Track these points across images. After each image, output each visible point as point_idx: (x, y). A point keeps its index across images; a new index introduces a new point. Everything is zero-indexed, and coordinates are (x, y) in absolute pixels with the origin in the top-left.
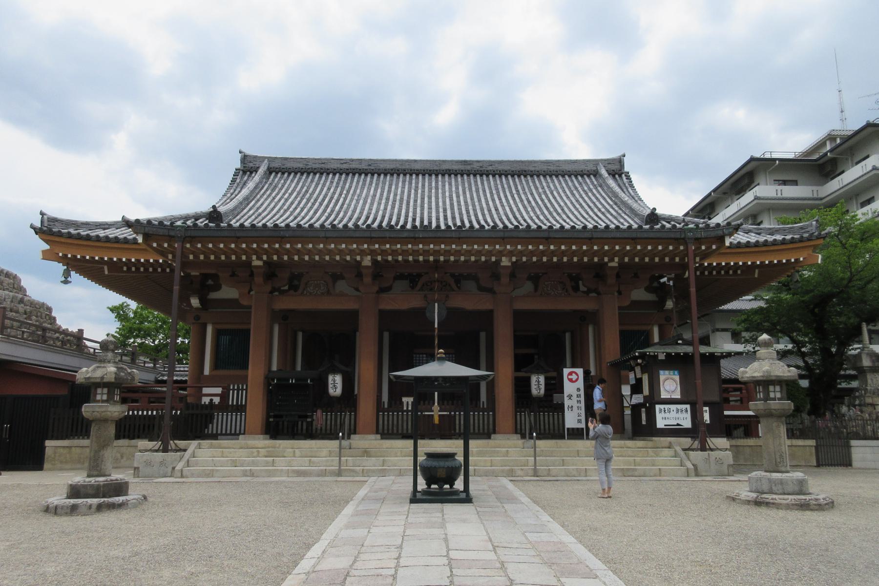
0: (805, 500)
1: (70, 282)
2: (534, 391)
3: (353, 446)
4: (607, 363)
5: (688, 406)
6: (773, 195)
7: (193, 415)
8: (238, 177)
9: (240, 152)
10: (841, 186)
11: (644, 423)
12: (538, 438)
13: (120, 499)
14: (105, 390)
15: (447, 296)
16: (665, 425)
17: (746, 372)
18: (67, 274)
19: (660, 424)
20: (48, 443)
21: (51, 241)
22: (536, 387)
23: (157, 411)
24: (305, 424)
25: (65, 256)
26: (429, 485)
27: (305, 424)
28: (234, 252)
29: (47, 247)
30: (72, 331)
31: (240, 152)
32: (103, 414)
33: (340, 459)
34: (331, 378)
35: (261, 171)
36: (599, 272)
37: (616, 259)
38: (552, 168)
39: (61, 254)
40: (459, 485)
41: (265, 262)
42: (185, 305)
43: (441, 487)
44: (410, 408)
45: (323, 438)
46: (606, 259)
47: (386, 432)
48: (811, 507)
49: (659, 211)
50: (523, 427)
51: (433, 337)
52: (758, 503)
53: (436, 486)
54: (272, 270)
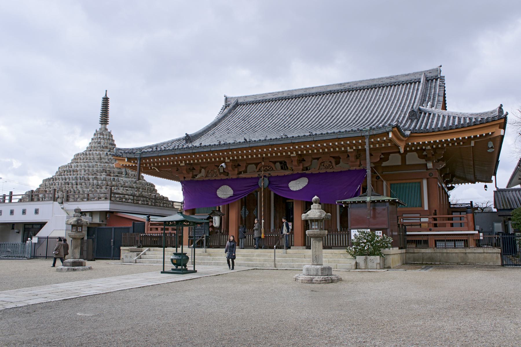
3: (287, 252)
20: (122, 248)
23: (158, 234)
28: (337, 146)
38: (393, 80)
41: (231, 160)
46: (289, 153)
49: (189, 133)
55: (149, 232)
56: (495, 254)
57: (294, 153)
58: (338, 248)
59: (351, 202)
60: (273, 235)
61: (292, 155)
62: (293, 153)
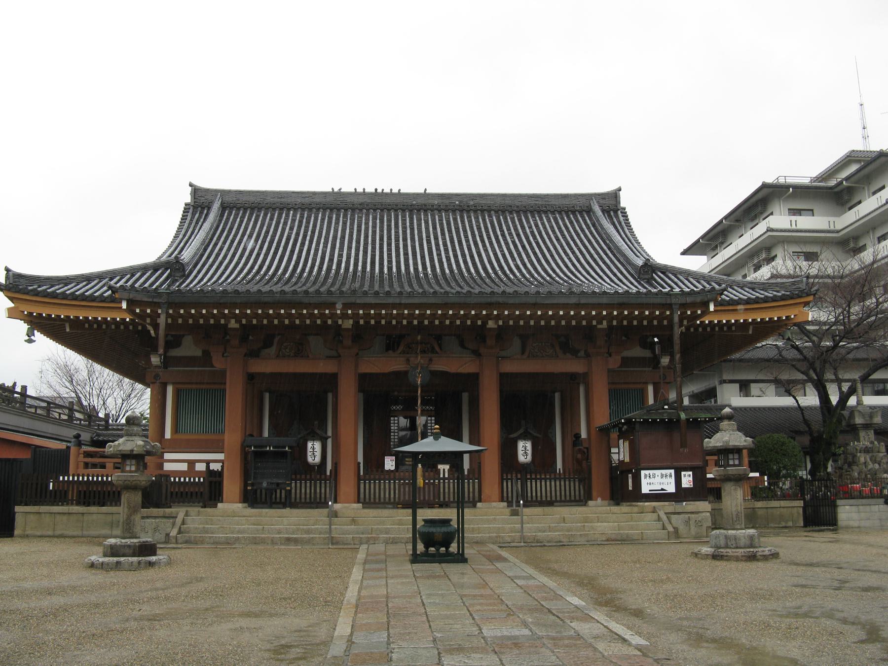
0: (753, 552)
1: (35, 341)
2: (522, 458)
4: (596, 428)
5: (672, 471)
6: (787, 226)
7: (215, 482)
8: (189, 214)
9: (191, 185)
10: (858, 218)
11: (630, 488)
12: (525, 506)
13: (153, 558)
14: (134, 462)
15: (431, 360)
16: (650, 491)
17: (710, 442)
18: (30, 334)
19: (645, 489)
20: (17, 509)
21: (14, 298)
22: (522, 452)
23: (88, 476)
24: (283, 492)
25: (31, 314)
26: (427, 547)
27: (283, 492)
29: (11, 305)
30: (8, 386)
31: (191, 185)
32: (134, 482)
33: (330, 527)
34: (310, 444)
35: (216, 206)
36: (588, 333)
37: (605, 322)
39: (26, 313)
40: (454, 548)
42: (143, 362)
43: (438, 550)
44: (446, 476)
45: (302, 507)
46: (594, 323)
47: (367, 500)
48: (757, 558)
50: (510, 495)
51: (417, 396)
52: (715, 557)
53: (433, 549)
54: (246, 331)
55: (81, 470)
56: (795, 508)
57: (605, 322)
58: (567, 504)
59: (705, 418)
60: (434, 481)
61: (599, 326)
62: (602, 323)
